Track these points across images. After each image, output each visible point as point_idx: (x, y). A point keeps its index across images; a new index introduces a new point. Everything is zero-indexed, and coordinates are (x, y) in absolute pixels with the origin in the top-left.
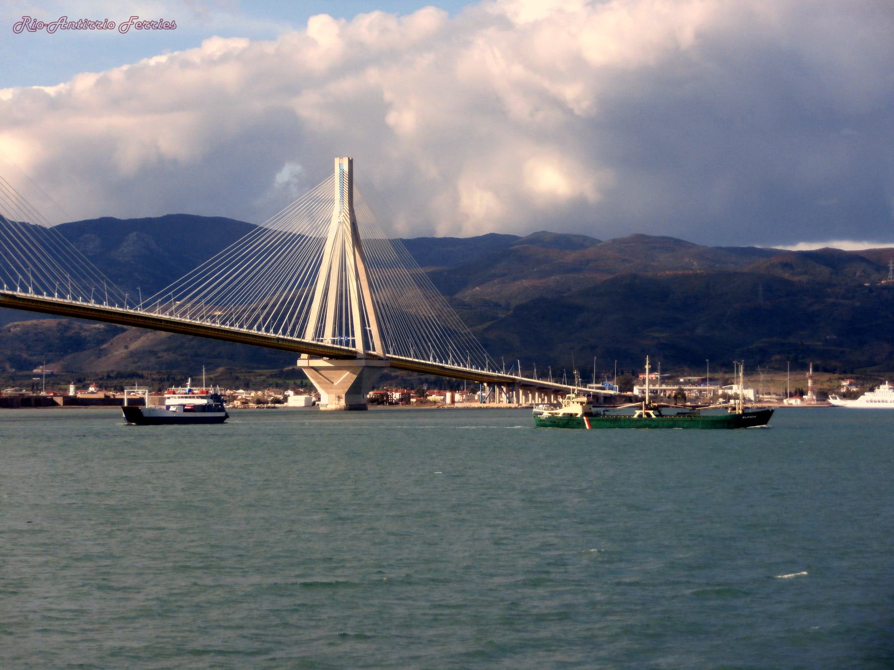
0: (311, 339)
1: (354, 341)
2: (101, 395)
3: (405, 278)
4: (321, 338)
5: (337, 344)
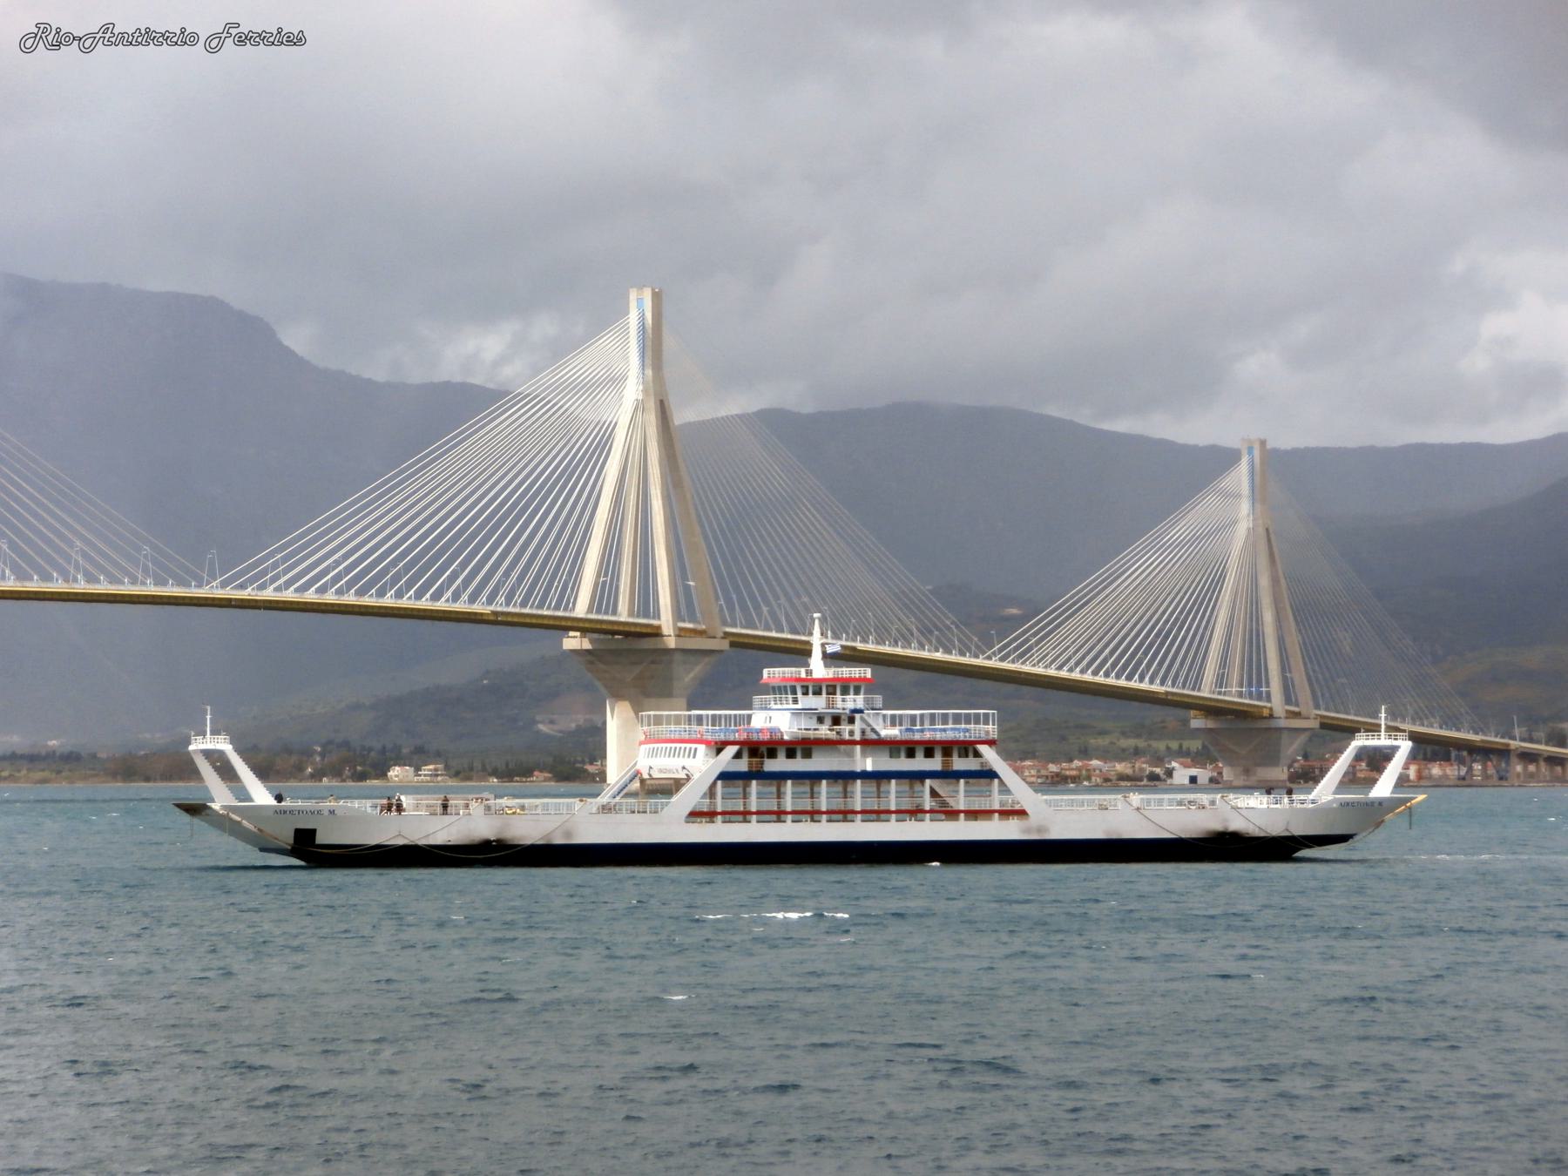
1: (1268, 695)
3: (1181, 594)
4: (1223, 690)
5: (1245, 698)
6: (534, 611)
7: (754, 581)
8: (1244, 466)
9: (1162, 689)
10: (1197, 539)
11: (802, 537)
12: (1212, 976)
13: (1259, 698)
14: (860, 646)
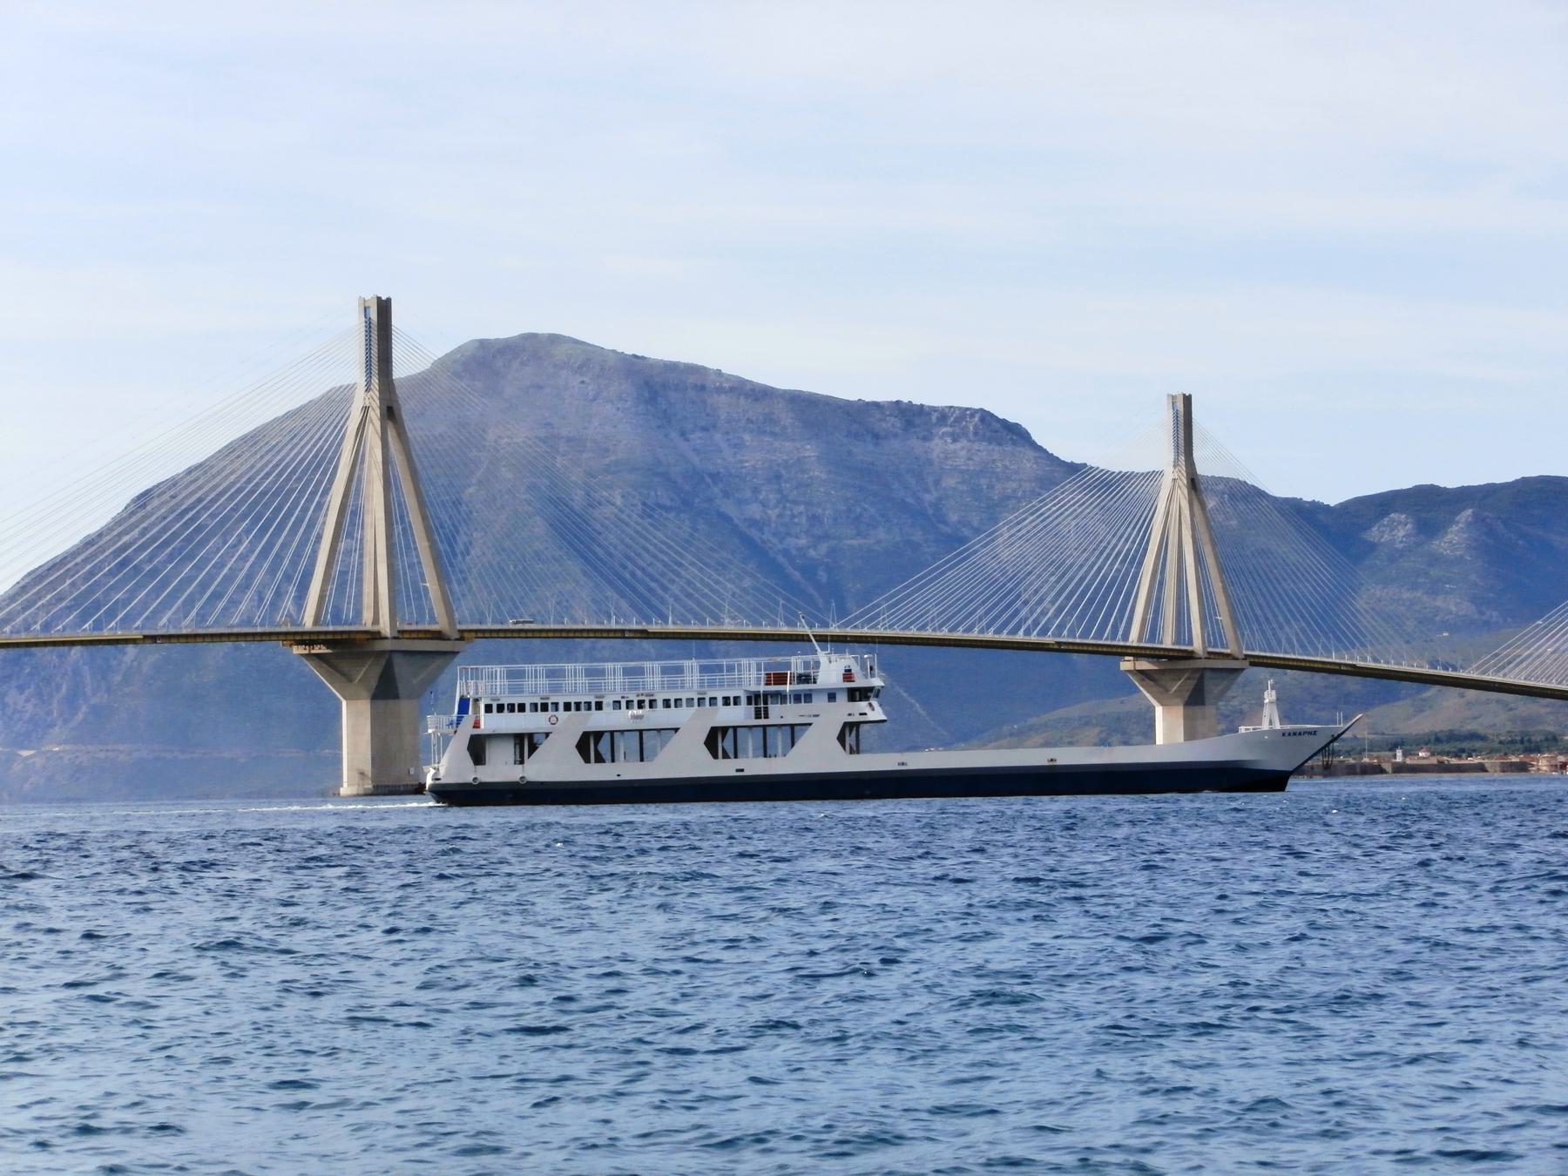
0: (1136, 640)
2: (1434, 761)
6: (1108, 643)
11: (1269, 584)
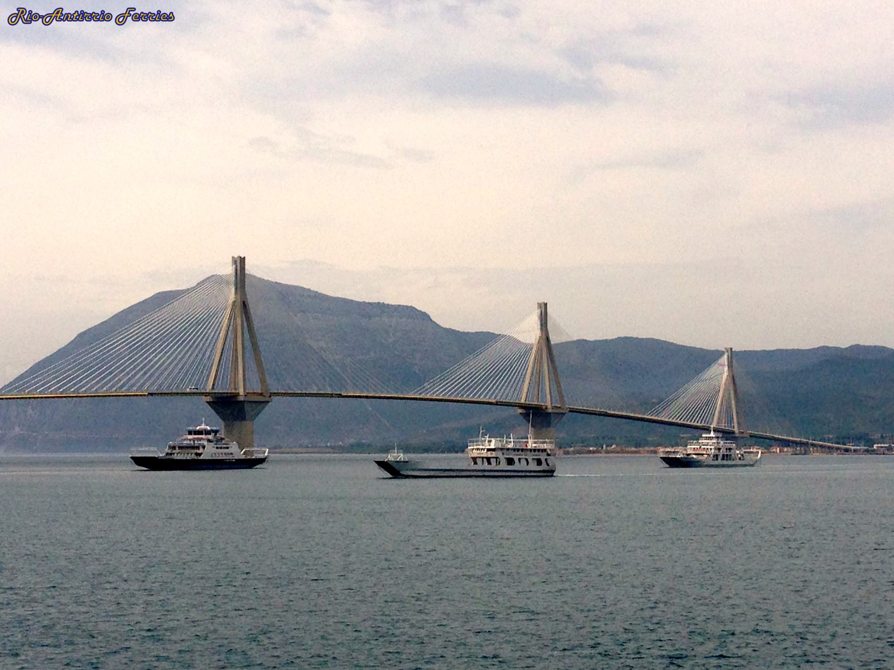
7: (100, 379)
8: (725, 356)
9: (701, 425)
10: (491, 377)
12: (387, 478)
13: (731, 427)
14: (609, 412)
